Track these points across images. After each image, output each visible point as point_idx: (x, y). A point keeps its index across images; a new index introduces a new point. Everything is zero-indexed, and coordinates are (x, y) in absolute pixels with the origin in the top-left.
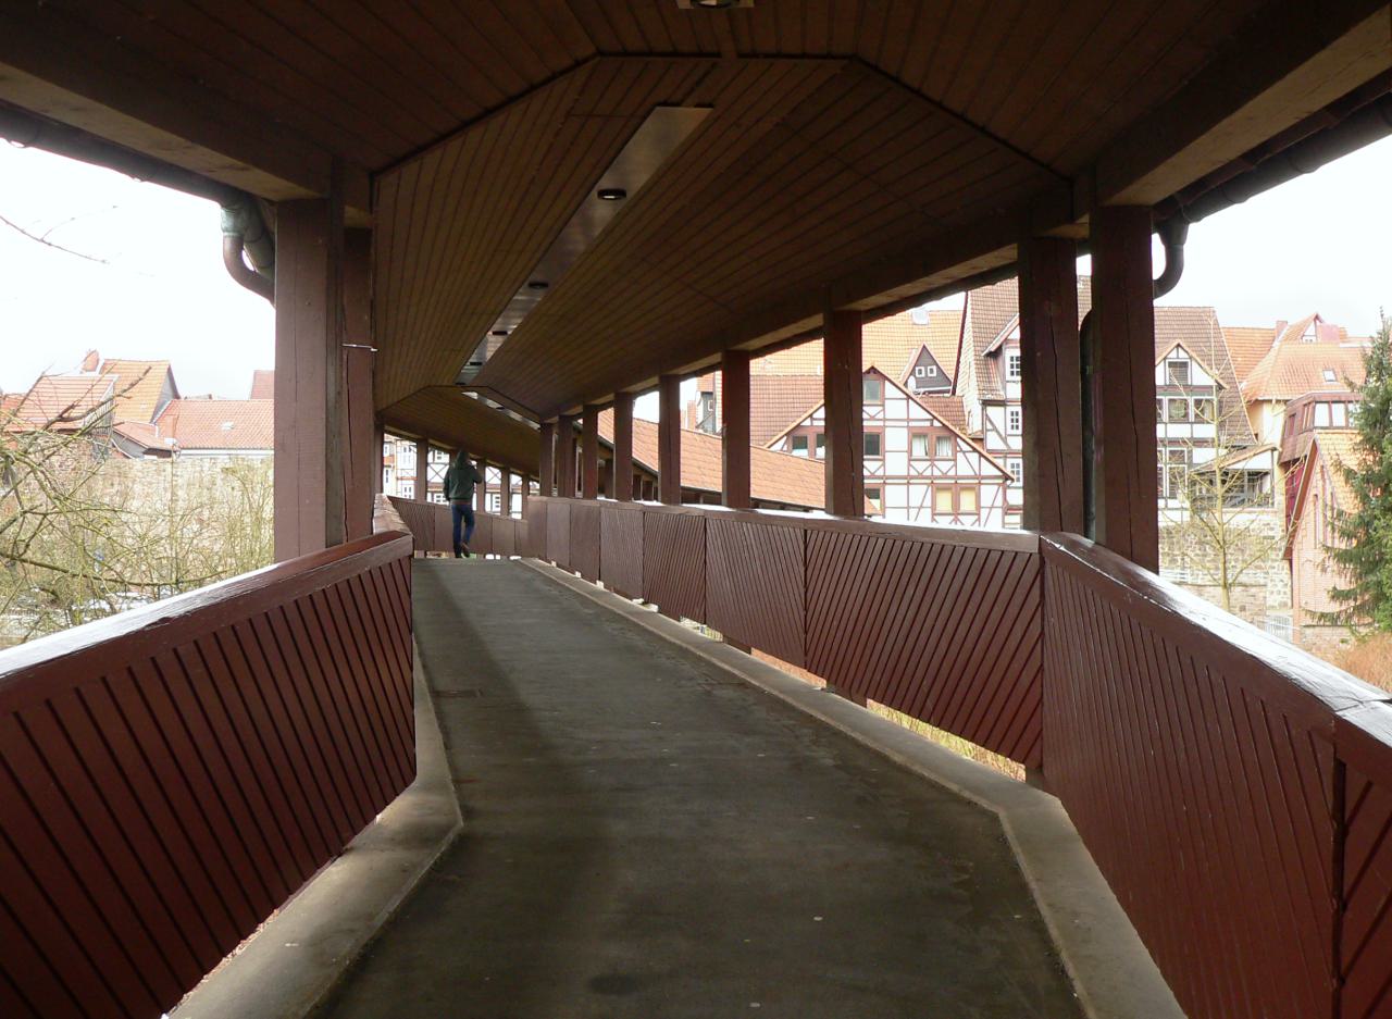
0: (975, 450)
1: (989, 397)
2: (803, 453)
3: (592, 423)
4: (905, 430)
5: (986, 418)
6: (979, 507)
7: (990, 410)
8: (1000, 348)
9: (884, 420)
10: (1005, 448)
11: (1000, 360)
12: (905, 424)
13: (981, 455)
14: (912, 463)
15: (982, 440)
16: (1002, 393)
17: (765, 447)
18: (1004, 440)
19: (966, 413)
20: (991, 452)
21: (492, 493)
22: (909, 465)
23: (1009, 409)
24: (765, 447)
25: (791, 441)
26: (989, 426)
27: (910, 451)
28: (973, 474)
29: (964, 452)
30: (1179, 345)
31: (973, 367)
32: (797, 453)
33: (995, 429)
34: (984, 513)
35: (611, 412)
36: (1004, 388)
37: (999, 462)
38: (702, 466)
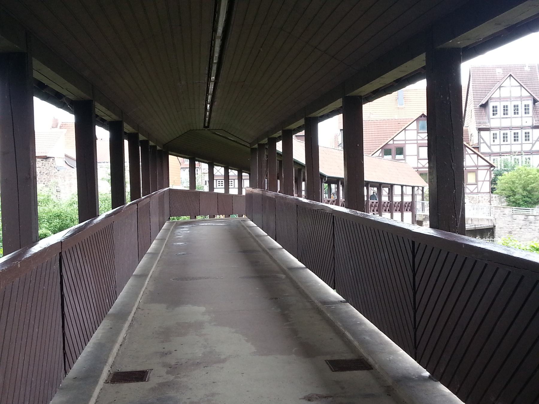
0: (475, 153)
1: (481, 127)
2: (390, 157)
3: (288, 147)
4: (416, 145)
5: (480, 137)
6: (477, 181)
7: (482, 132)
8: (488, 101)
9: (405, 140)
10: (490, 151)
11: (487, 108)
12: (416, 142)
13: (478, 155)
14: (419, 161)
15: (478, 148)
16: (488, 124)
17: (370, 155)
18: (489, 147)
19: (470, 135)
20: (483, 154)
21: (216, 180)
22: (418, 162)
23: (492, 132)
24: (370, 155)
25: (383, 150)
26: (482, 141)
27: (418, 155)
28: (474, 165)
29: (470, 154)
30: (510, 75)
31: (473, 112)
32: (385, 157)
33: (485, 142)
34: (480, 184)
35: (281, 142)
36: (489, 122)
37: (487, 158)
38: (332, 163)
